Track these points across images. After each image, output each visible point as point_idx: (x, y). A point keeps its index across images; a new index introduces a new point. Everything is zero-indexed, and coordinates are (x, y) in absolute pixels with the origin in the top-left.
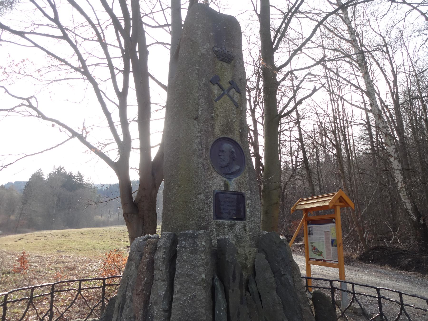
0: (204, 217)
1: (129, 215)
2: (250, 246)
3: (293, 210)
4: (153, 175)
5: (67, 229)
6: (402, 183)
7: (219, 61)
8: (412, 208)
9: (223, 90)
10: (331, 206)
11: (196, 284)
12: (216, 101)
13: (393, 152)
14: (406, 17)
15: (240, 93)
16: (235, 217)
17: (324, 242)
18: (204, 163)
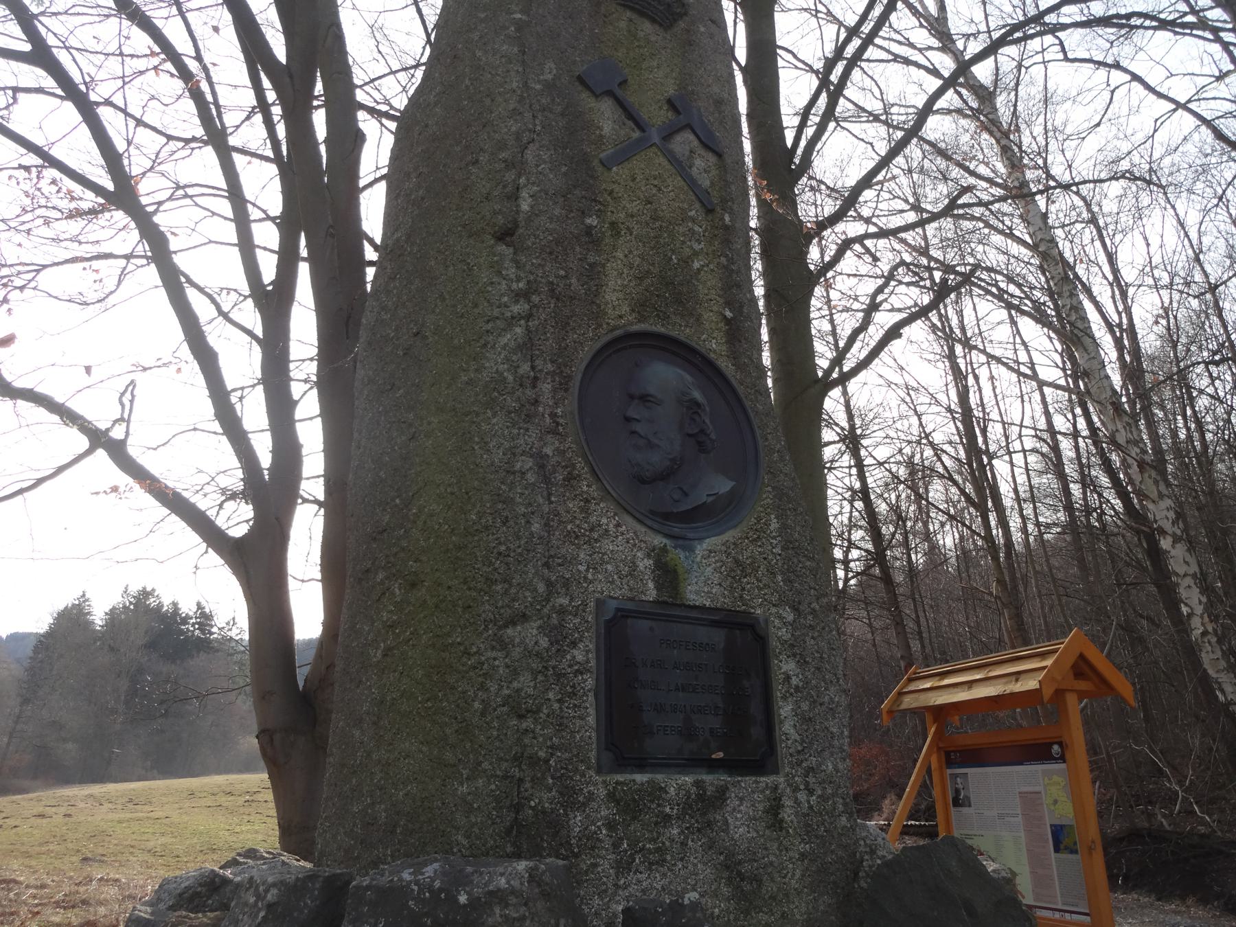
0: (542, 754)
3: (890, 712)
5: (154, 779)
6: (1206, 619)
7: (619, 8)
9: (639, 126)
10: (1048, 693)
12: (606, 165)
13: (1168, 519)
14: (1155, 131)
15: (719, 155)
16: (721, 755)
17: (1022, 834)
18: (548, 451)
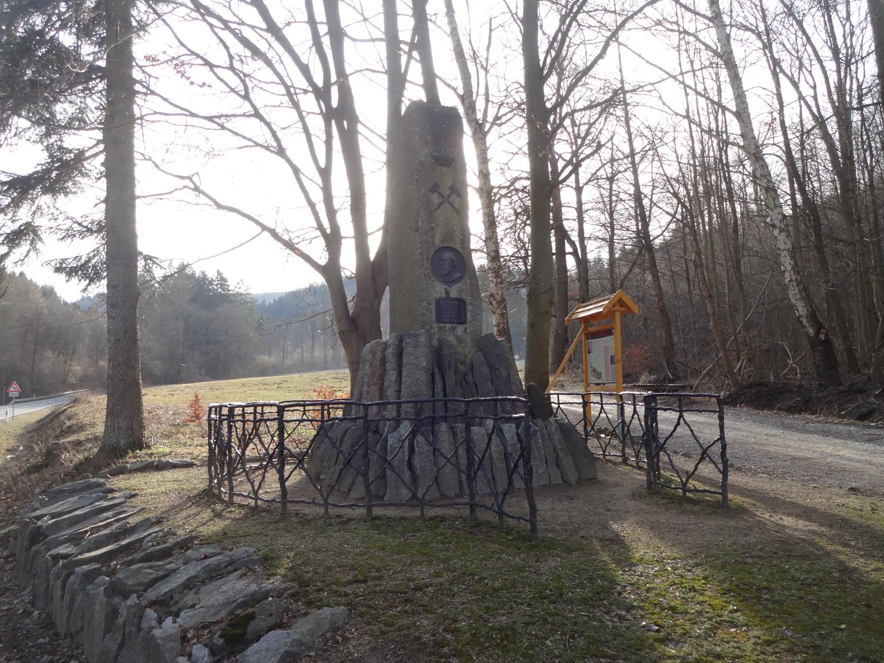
1: (346, 334)
2: (471, 347)
4: (374, 280)
6: (792, 273)
8: (806, 315)
9: (443, 197)
11: (419, 370)
12: (435, 210)
